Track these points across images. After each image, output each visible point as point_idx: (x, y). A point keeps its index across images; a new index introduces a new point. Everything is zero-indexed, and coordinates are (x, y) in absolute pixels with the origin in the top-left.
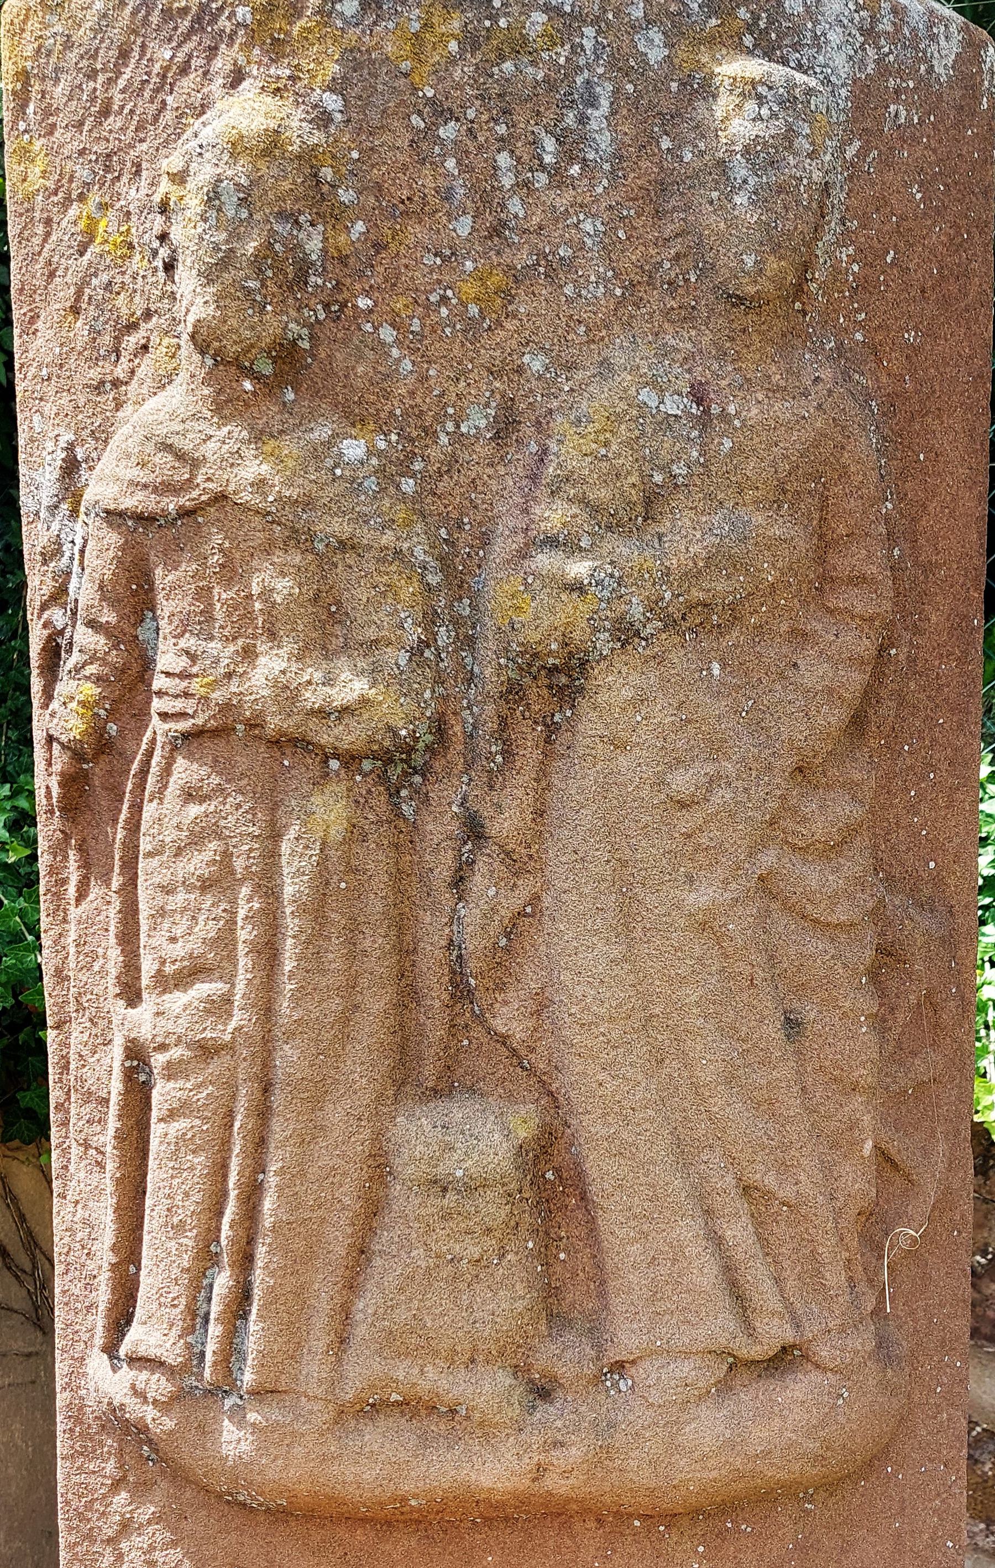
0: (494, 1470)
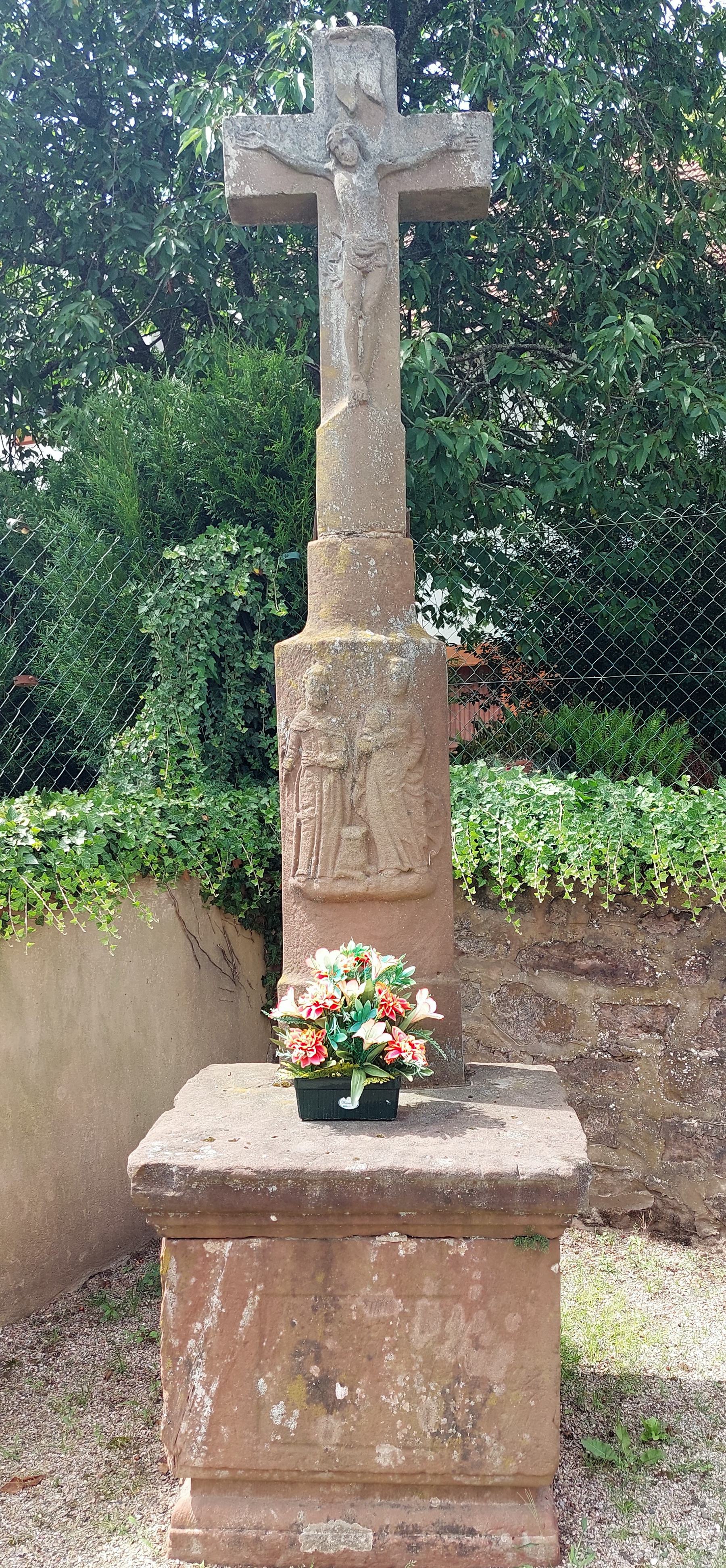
0: (359, 888)
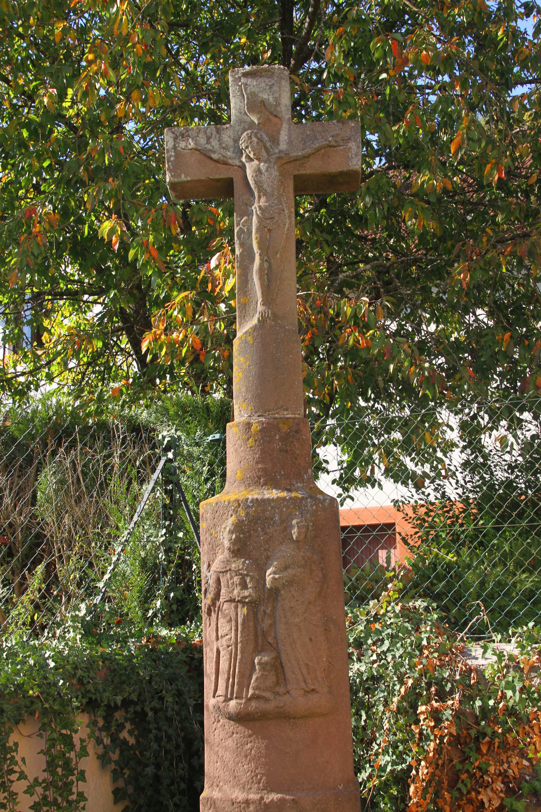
0: (269, 707)
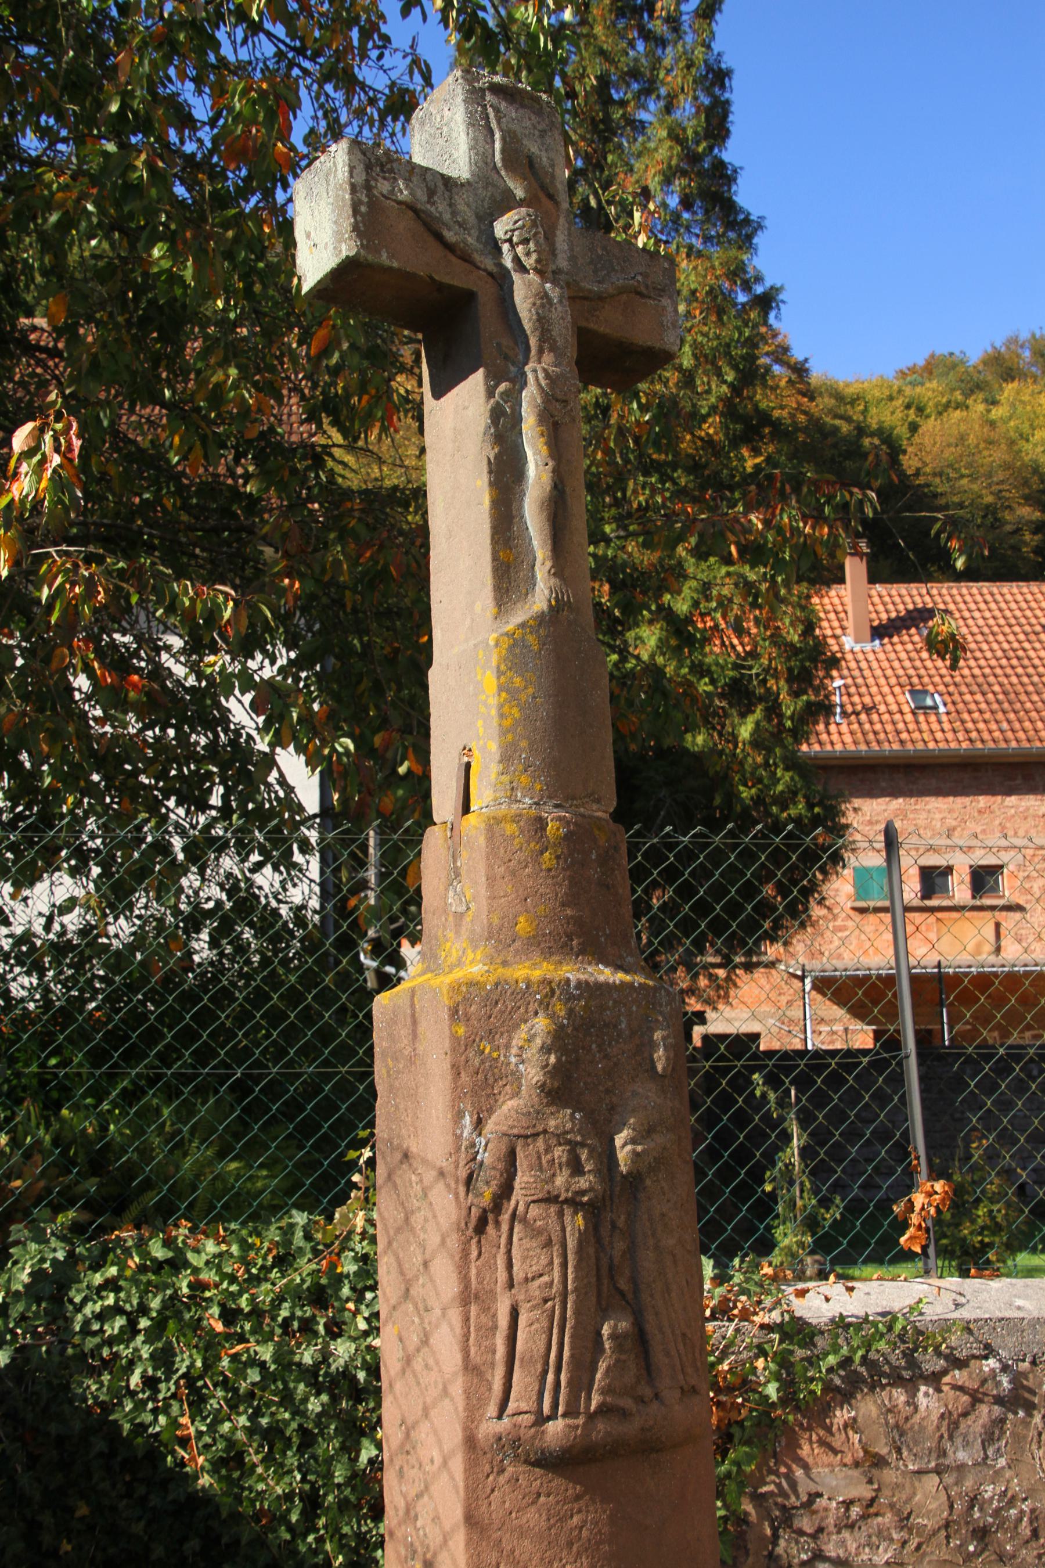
0: (630, 1429)
